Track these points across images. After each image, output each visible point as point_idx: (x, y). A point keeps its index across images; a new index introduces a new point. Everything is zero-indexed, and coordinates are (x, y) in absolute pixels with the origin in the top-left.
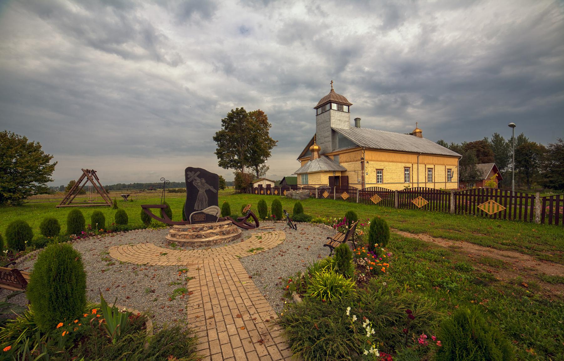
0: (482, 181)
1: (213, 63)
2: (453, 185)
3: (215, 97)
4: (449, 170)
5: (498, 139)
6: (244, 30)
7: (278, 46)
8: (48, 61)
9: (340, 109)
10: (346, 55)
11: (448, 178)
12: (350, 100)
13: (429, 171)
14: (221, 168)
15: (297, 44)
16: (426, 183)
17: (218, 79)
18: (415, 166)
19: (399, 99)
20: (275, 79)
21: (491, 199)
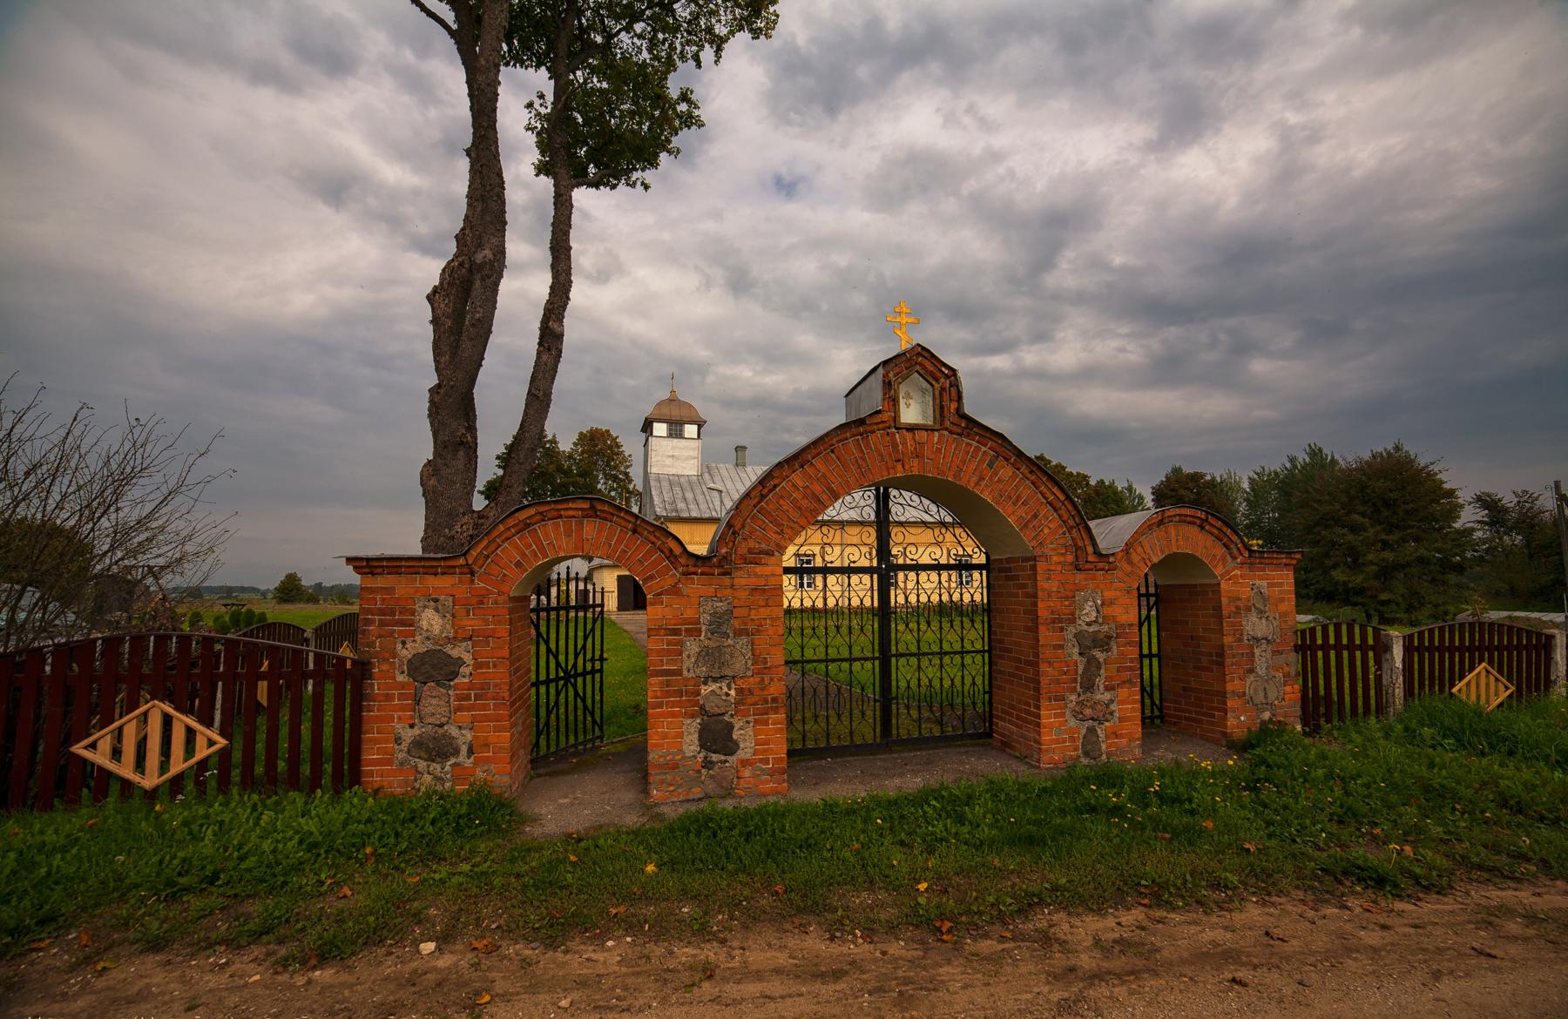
1: (696, 268)
3: (703, 353)
6: (786, 186)
7: (866, 216)
9: (676, 432)
10: (1057, 224)
12: (703, 411)
14: (287, 607)
15: (915, 208)
17: (710, 307)
19: (1222, 337)
20: (859, 300)
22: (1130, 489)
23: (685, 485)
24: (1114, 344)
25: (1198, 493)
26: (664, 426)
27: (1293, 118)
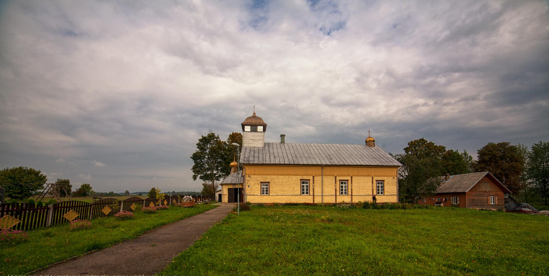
9: (254, 129)
21: (7, 214)
22: (465, 154)
23: (257, 151)
25: (504, 152)
26: (249, 127)
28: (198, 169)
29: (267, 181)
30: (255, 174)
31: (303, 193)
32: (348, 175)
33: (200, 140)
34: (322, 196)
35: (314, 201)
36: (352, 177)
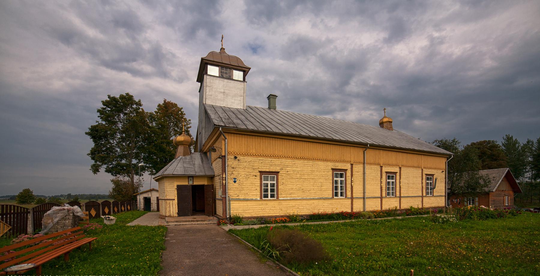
0: (487, 194)
2: (438, 200)
4: (430, 177)
5: (510, 142)
8: (69, 81)
10: (351, 68)
11: (427, 189)
13: (389, 177)
16: (381, 198)
18: (358, 168)
24: (369, 112)
27: (436, 34)
28: (100, 156)
29: (273, 169)
30: (247, 155)
31: (336, 195)
32: (396, 165)
33: (104, 103)
34: (364, 198)
35: (352, 208)
36: (400, 168)
